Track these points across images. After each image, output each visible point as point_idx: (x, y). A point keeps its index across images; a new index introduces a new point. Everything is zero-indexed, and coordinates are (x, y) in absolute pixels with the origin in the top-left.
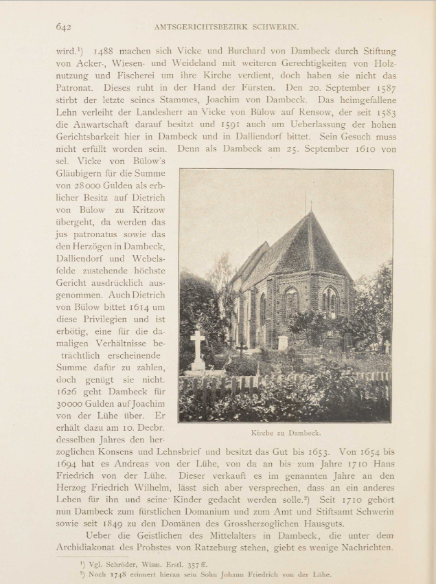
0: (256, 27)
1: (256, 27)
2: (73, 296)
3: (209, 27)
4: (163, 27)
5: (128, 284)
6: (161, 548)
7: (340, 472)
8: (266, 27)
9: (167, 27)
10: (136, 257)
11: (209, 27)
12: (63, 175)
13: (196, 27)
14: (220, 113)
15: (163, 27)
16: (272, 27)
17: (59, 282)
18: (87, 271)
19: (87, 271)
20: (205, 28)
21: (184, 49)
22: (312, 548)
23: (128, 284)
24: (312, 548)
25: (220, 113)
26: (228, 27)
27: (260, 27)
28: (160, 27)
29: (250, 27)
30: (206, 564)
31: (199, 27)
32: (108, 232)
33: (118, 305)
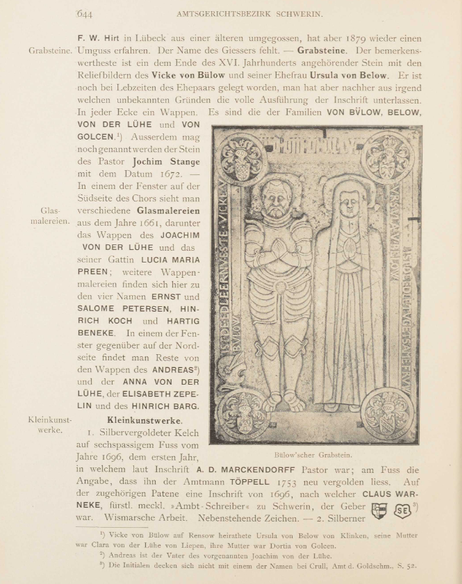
0: (280, 14)
1: (280, 14)
2: (146, 199)
3: (231, 14)
4: (186, 14)
5: (159, 506)
6: (285, 519)
7: (249, 59)
8: (289, 14)
9: (190, 14)
10: (108, 516)
11: (231, 14)
12: (144, 212)
13: (218, 14)
14: (132, 113)
15: (186, 14)
16: (296, 14)
17: (344, 506)
18: (261, 507)
19: (261, 507)
20: (227, 15)
21: (158, 73)
22: (241, 39)
23: (159, 506)
24: (241, 39)
25: (132, 113)
26: (252, 14)
27: (284, 14)
28: (182, 13)
29: (273, 14)
30: (114, 308)
31: (222, 14)
32: (154, 419)
33: (140, 270)
